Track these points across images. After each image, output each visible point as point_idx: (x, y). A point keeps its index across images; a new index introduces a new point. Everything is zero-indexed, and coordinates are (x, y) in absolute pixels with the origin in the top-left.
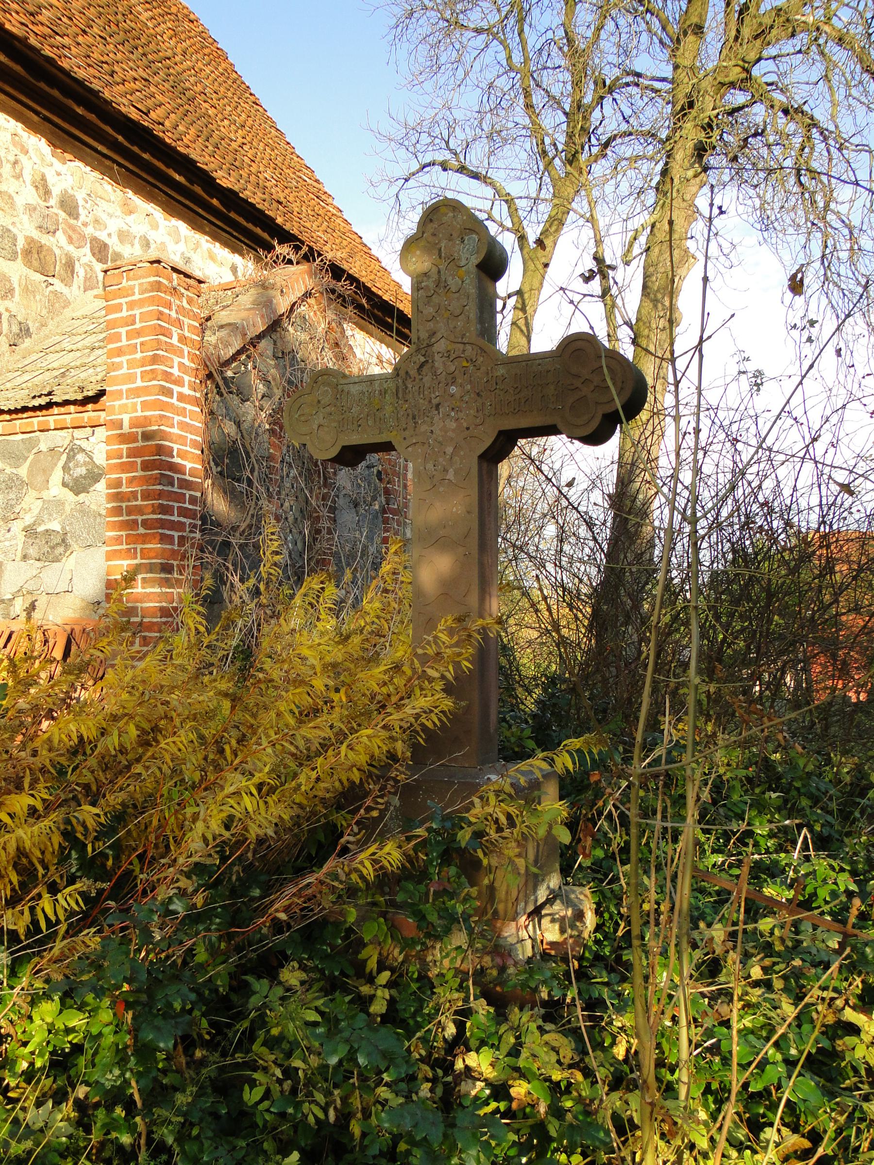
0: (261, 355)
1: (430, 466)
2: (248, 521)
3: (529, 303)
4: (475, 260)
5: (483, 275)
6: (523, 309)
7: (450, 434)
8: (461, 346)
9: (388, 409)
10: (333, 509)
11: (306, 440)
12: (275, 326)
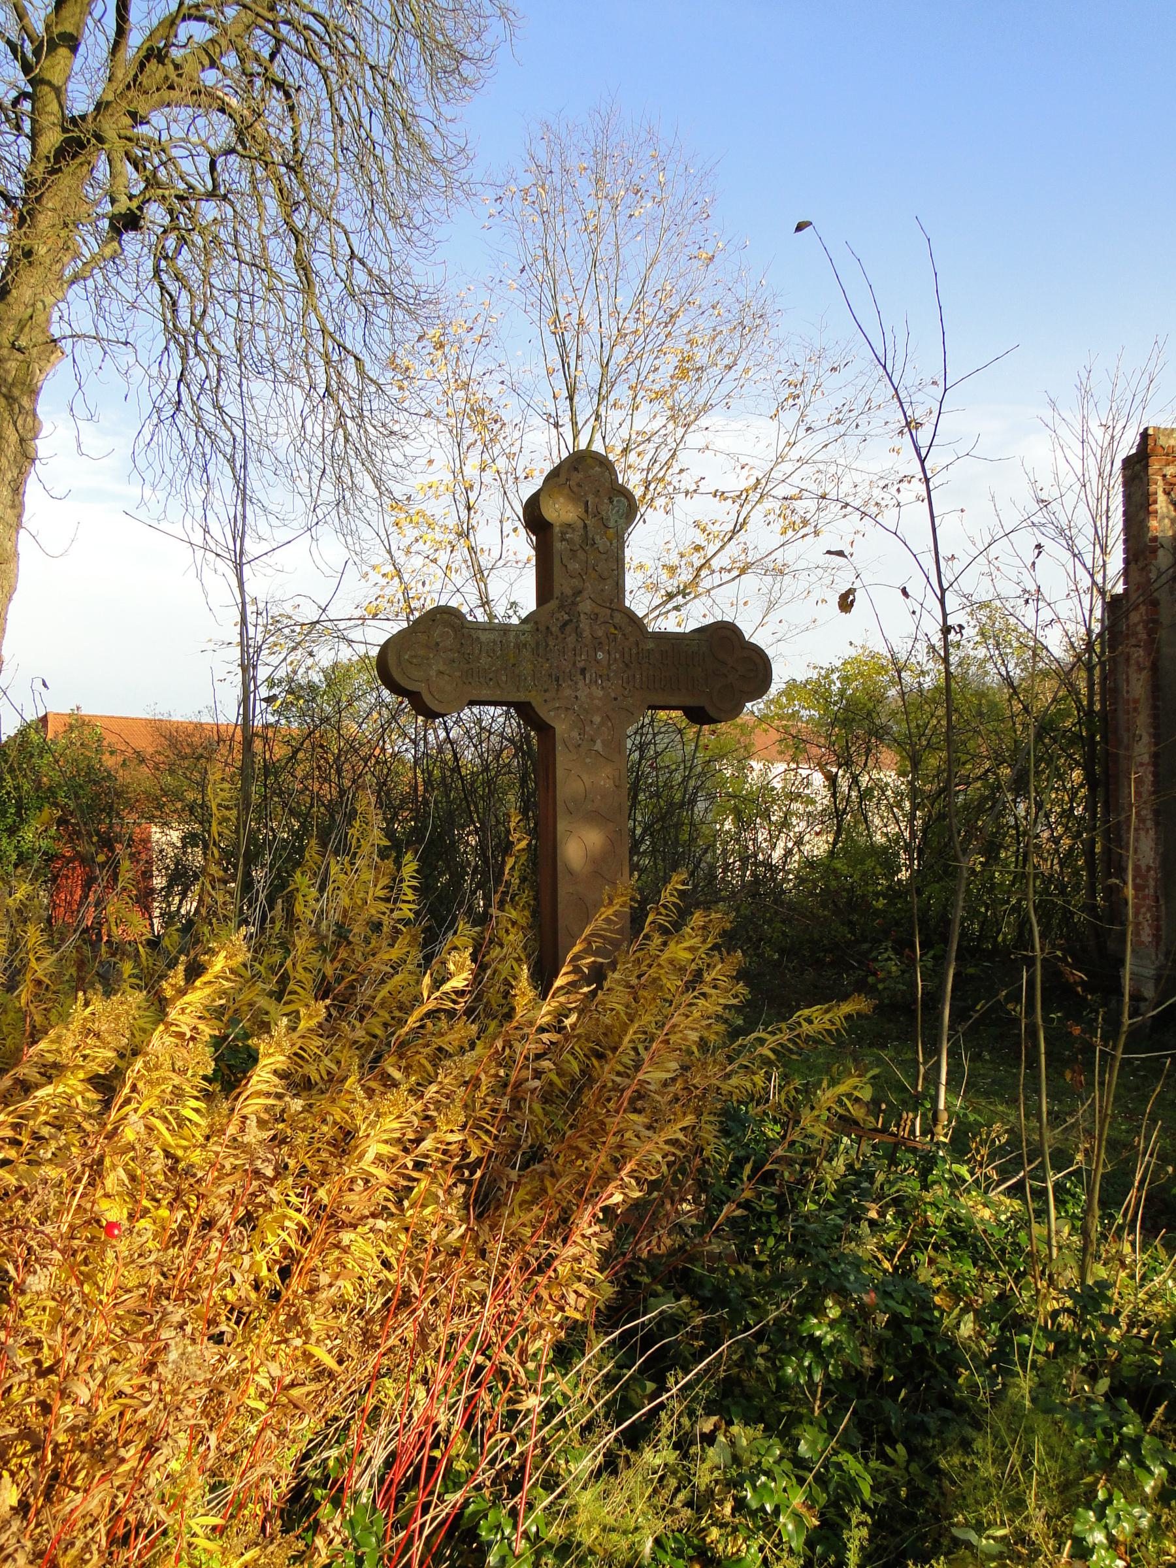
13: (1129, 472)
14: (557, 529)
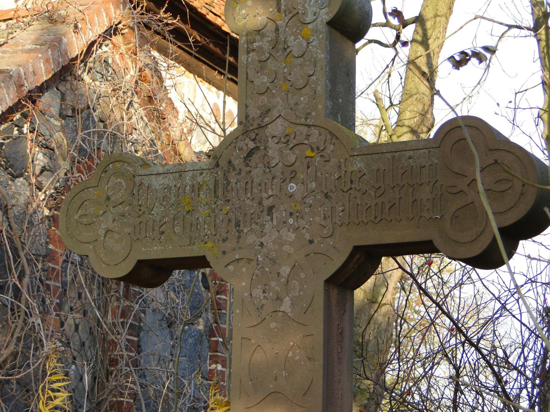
0: (42, 113)
1: (258, 292)
2: (12, 347)
3: (432, 34)
4: (326, 15)
5: (338, 35)
6: (425, 43)
7: (287, 248)
8: (304, 129)
9: (203, 212)
10: (135, 330)
11: (87, 250)
12: (65, 73)
13: (461, 123)
14: (242, 41)
